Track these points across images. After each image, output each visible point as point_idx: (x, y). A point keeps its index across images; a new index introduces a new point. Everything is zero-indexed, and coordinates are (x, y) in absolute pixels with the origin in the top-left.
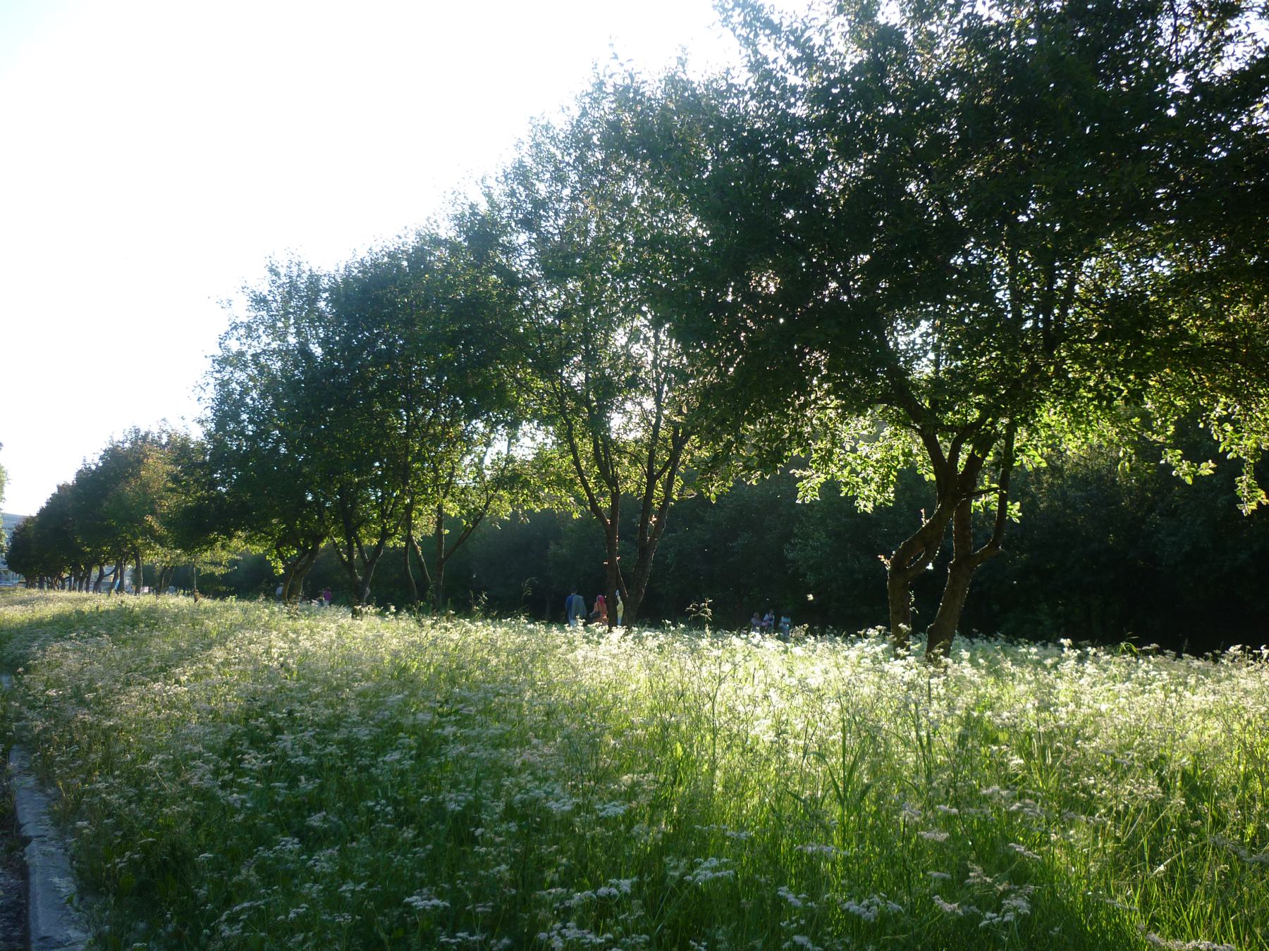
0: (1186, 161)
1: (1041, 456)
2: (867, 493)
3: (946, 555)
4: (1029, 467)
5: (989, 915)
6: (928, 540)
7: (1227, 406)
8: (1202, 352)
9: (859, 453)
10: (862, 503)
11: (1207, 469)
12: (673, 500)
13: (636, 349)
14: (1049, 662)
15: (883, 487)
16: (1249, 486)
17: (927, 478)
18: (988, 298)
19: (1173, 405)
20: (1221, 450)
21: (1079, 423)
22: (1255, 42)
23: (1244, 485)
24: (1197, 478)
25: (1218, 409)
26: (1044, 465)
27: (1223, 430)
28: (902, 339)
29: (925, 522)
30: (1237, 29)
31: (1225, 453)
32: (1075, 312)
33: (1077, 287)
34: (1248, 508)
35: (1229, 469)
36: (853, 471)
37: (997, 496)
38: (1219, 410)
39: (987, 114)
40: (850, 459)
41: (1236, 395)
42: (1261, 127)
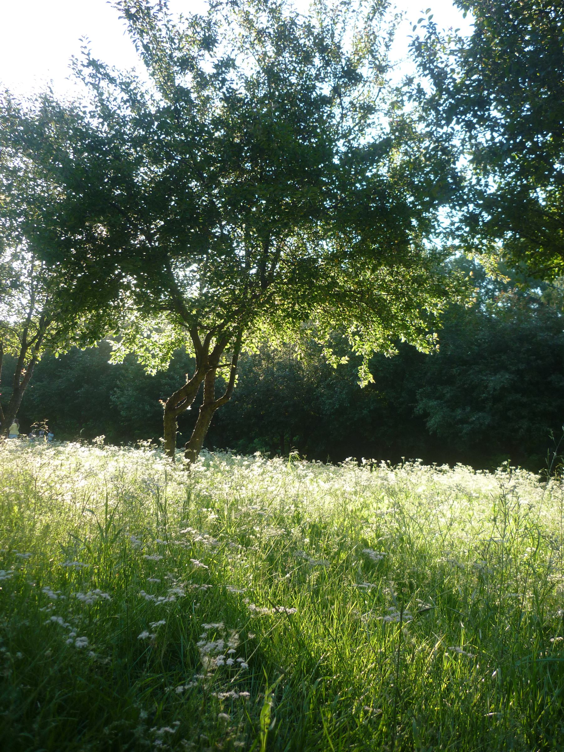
0: (342, 187)
1: (257, 348)
2: (153, 364)
3: (199, 401)
4: (250, 354)
5: (160, 598)
6: (188, 392)
7: (357, 326)
8: (345, 295)
9: (151, 339)
10: (149, 369)
11: (344, 360)
12: (38, 361)
13: (16, 265)
14: (246, 463)
15: (163, 360)
16: (365, 372)
17: (191, 356)
18: (230, 252)
19: (329, 323)
20: (353, 350)
21: (279, 330)
22: (382, 129)
23: (362, 371)
24: (340, 366)
25: (353, 328)
26: (258, 353)
27: (355, 339)
28: (181, 274)
29: (188, 381)
30: (373, 121)
31: (355, 352)
32: (280, 267)
33: (282, 253)
34: (363, 384)
35: (356, 361)
36: (147, 349)
37: (228, 369)
38: (353, 329)
39: (238, 148)
40: (145, 342)
41: (362, 320)
42: (382, 176)
